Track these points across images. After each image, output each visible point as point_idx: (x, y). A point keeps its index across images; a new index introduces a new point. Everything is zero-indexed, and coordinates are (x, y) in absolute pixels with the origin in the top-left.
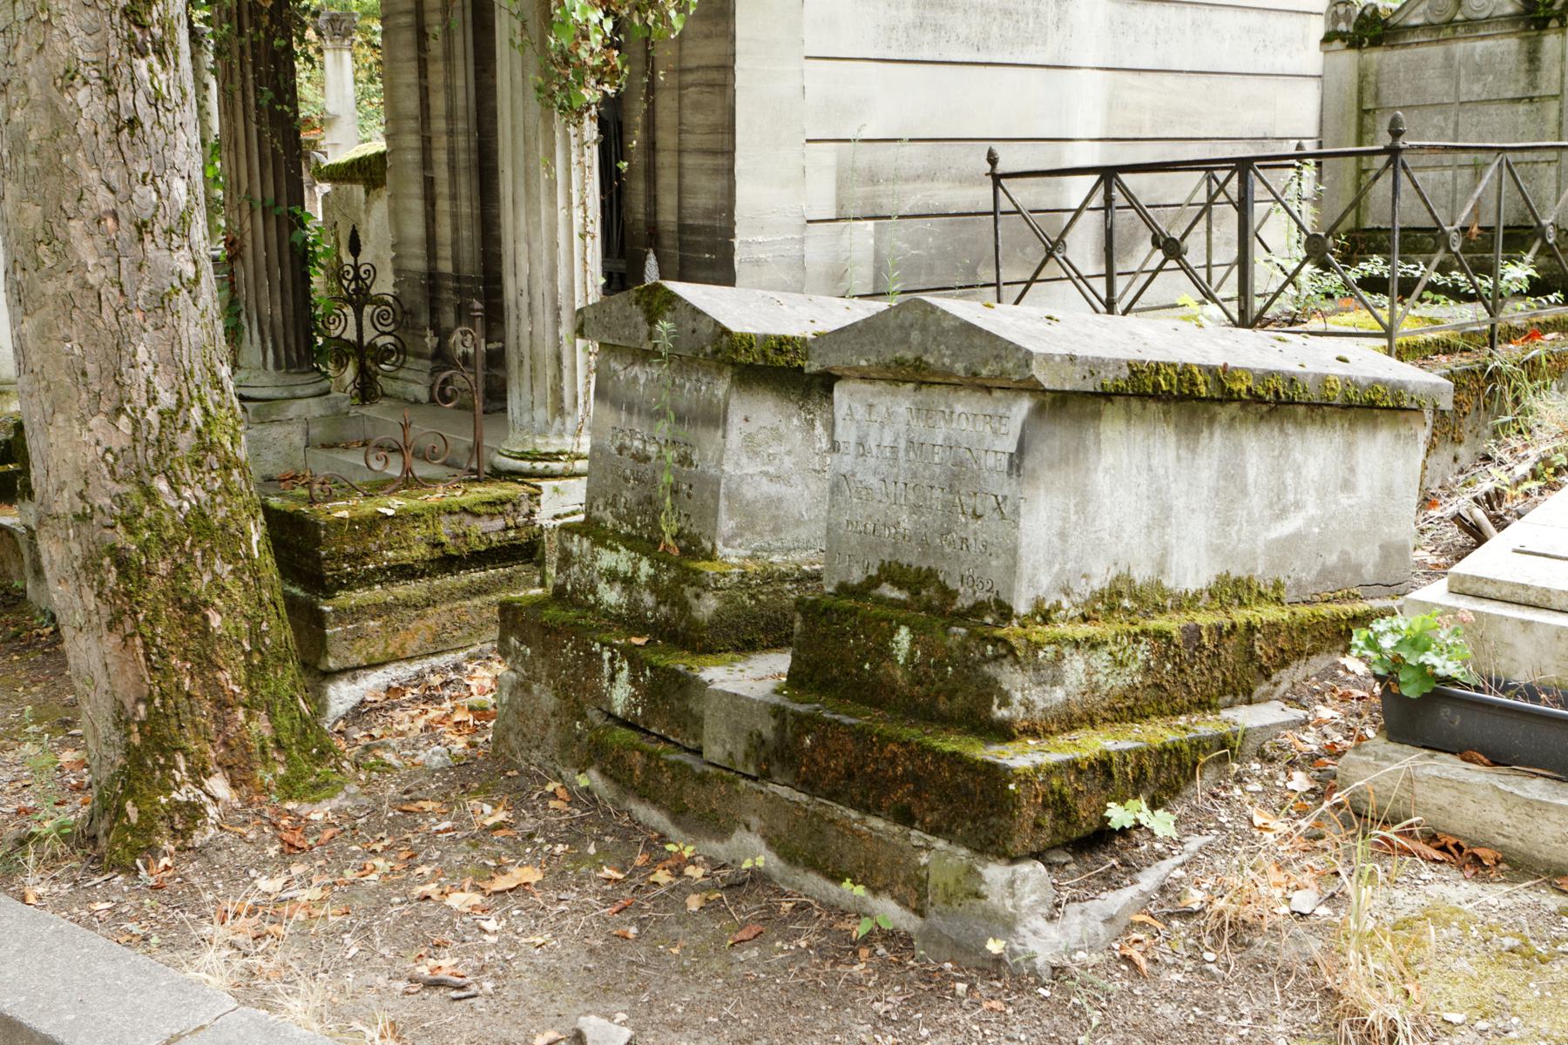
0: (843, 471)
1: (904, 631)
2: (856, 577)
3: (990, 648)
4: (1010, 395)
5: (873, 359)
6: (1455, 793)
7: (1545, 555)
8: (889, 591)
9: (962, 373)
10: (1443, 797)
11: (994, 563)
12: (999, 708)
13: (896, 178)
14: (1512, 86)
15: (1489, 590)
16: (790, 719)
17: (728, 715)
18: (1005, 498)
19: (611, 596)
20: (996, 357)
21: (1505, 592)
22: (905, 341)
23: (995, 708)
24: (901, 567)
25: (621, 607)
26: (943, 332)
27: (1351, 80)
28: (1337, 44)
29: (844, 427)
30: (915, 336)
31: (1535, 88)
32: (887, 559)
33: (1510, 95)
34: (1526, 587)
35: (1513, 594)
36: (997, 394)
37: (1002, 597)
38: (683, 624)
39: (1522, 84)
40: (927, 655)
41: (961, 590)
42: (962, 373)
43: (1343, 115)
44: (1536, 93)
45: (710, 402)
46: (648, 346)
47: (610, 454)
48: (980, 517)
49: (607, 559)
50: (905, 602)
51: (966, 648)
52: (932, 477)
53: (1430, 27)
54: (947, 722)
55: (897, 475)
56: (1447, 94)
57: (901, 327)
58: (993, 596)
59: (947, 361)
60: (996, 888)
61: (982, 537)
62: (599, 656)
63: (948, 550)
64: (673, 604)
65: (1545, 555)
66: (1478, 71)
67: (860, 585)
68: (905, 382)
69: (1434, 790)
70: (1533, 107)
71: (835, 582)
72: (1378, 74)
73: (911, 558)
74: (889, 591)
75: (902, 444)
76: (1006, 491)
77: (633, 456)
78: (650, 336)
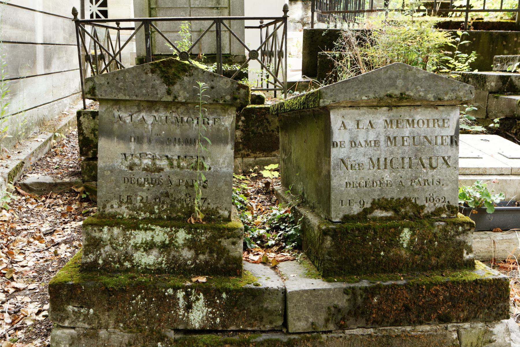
0: (341, 157)
1: (406, 230)
2: (356, 209)
3: (460, 228)
4: (449, 108)
5: (372, 96)
6: (508, 243)
7: (469, 158)
8: (379, 213)
9: (432, 99)
10: (504, 246)
11: (445, 189)
12: (467, 254)
14: (210, 3)
15: (467, 172)
16: (359, 292)
17: (310, 302)
18: (449, 157)
19: (149, 259)
20: (452, 90)
21: (472, 171)
22: (393, 85)
23: (465, 255)
24: (386, 200)
25: (161, 263)
26: (418, 79)
29: (339, 134)
30: (400, 83)
31: (219, 4)
32: (377, 198)
33: (210, 6)
34: (479, 168)
35: (475, 172)
36: (441, 108)
37: (451, 204)
38: (222, 262)
39: (214, 2)
40: (422, 239)
41: (427, 205)
42: (432, 99)
43: (143, 9)
44: (220, 6)
45: (218, 130)
46: (170, 99)
47: (121, 171)
48: (435, 168)
49: (140, 237)
50: (390, 217)
51: (446, 231)
52: (404, 153)
54: (440, 268)
55: (380, 155)
56: (185, 4)
57: (390, 78)
58: (446, 204)
59: (422, 94)
60: (501, 335)
61: (436, 178)
62: (174, 297)
63: (416, 187)
64: (211, 252)
65: (469, 158)
67: (359, 214)
68: (381, 107)
69: (501, 244)
70: (219, 11)
71: (341, 215)
73: (393, 194)
74: (379, 213)
75: (382, 139)
76: (450, 154)
77: (144, 169)
78: (169, 93)
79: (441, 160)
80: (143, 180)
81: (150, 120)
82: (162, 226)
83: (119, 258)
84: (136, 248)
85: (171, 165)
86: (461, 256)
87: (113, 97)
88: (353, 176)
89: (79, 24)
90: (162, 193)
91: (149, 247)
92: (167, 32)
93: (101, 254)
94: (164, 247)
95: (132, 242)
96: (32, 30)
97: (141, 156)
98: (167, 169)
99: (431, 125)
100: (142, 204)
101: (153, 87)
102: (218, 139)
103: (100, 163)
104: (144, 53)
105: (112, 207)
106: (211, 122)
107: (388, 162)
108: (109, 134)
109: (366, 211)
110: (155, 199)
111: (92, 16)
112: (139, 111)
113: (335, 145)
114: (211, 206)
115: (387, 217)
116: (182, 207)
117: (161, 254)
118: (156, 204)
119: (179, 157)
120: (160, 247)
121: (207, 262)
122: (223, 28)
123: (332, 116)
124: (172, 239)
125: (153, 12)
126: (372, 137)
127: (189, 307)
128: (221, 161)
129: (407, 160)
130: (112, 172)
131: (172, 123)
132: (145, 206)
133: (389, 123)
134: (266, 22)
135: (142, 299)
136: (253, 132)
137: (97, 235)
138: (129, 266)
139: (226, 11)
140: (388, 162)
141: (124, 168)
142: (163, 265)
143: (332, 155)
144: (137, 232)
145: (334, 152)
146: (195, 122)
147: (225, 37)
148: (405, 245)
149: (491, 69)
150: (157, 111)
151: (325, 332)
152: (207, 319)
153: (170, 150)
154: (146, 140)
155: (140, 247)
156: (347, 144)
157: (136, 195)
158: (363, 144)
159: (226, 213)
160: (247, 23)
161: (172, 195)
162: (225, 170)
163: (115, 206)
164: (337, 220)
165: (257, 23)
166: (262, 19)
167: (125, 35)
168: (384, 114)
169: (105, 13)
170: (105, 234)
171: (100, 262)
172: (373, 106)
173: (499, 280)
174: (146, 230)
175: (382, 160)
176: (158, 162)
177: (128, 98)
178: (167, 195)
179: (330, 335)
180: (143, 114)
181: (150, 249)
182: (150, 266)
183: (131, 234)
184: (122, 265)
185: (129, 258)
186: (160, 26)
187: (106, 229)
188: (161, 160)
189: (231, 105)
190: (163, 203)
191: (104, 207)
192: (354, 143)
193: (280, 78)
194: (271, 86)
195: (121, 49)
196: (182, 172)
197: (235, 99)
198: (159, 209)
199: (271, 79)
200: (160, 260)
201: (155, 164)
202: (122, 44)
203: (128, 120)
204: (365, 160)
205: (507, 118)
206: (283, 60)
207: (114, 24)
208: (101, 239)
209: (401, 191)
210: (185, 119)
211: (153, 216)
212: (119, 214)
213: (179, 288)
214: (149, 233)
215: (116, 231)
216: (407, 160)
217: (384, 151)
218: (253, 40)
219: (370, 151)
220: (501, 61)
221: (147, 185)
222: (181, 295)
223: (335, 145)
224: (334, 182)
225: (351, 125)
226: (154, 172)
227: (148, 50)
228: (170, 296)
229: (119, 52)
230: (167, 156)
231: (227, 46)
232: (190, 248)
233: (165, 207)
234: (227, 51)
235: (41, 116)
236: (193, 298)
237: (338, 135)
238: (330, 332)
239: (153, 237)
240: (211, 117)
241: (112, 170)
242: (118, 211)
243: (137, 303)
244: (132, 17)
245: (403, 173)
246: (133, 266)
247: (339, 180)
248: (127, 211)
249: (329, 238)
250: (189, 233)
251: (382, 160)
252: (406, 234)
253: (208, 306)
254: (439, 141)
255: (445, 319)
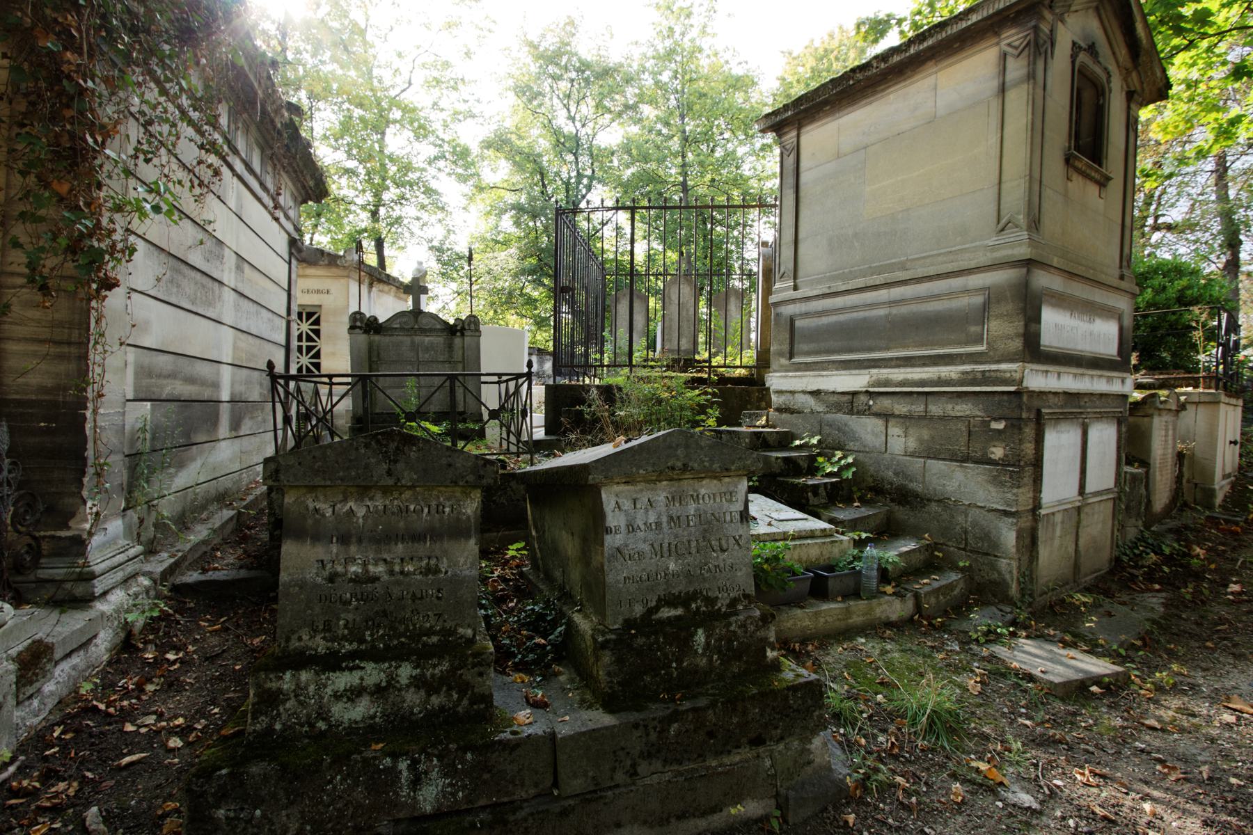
0: (616, 546)
1: (700, 631)
13: (159, 376)
27: (364, 348)
28: (357, 331)
45: (458, 519)
46: (390, 482)
47: (316, 586)
49: (342, 680)
52: (690, 535)
53: (402, 329)
61: (729, 562)
62: (393, 772)
63: (707, 575)
66: (427, 350)
72: (378, 347)
73: (680, 588)
74: (666, 613)
75: (664, 519)
76: (741, 532)
77: (351, 580)
79: (732, 541)
80: (348, 595)
81: (361, 512)
82: (376, 662)
83: (308, 716)
84: (337, 696)
85: (391, 573)
86: (765, 656)
87: (306, 483)
88: (632, 568)
89: (274, 377)
90: (377, 612)
91: (353, 694)
92: (390, 387)
93: (279, 715)
94: (379, 692)
95: (329, 690)
96: (216, 385)
97: (350, 560)
98: (386, 577)
99: (718, 500)
100: (346, 632)
101: (367, 467)
102: (457, 531)
103: (284, 577)
104: (360, 411)
105: (300, 639)
106: (447, 510)
107: (673, 547)
108: (300, 535)
109: (651, 611)
110: (367, 622)
111: (300, 369)
112: (345, 500)
113: (608, 531)
114: (448, 625)
115: (676, 617)
116: (407, 629)
117: (372, 702)
118: (368, 629)
119: (402, 560)
120: (372, 694)
121: (442, 708)
122: (457, 384)
123: (604, 496)
124: (392, 679)
125: (374, 366)
126: (652, 518)
127: (416, 783)
128: (462, 560)
129: (694, 544)
130: (301, 588)
131: (393, 513)
132: (351, 633)
133: (674, 498)
134: (504, 378)
135: (344, 779)
136: (494, 502)
137: (274, 685)
138: (323, 728)
139: (460, 366)
140: (673, 547)
141: (319, 580)
142: (377, 720)
143: (606, 544)
144: (338, 674)
145: (608, 539)
146: (426, 510)
147: (459, 392)
148: (700, 651)
149: (740, 425)
150: (371, 499)
151: (610, 788)
152: (444, 796)
153: (390, 551)
154: (354, 540)
155: (341, 696)
156: (623, 528)
157: (339, 619)
158: (642, 527)
159: (469, 632)
160: (483, 379)
161: (391, 613)
162: (467, 572)
163: (305, 637)
164: (616, 627)
165: (495, 379)
166: (500, 375)
167: (339, 390)
168: (664, 490)
169: (317, 366)
170: (287, 681)
171: (278, 727)
172: (889, 624)
173: (811, 683)
174: (351, 669)
175: (666, 545)
176: (371, 568)
177: (328, 483)
178: (385, 614)
179: (617, 791)
180: (351, 504)
181: (357, 696)
182: (356, 722)
183: (328, 678)
184: (312, 726)
185: (323, 714)
186: (382, 382)
187: (288, 675)
188: (376, 565)
189: (475, 487)
190: (379, 626)
191: (288, 640)
192: (631, 528)
193: (525, 437)
194: (513, 449)
195: (333, 406)
196: (408, 579)
197: (481, 477)
198: (372, 635)
199: (513, 439)
200: (372, 711)
201: (367, 571)
202: (335, 399)
203: (329, 513)
204: (646, 548)
205: (764, 476)
206: (528, 419)
207: (326, 380)
208: (280, 691)
209: (690, 582)
210: (412, 507)
211: (363, 647)
212: (311, 649)
213: (401, 755)
214: (357, 674)
215: (304, 676)
216: (694, 544)
217: (667, 535)
218: (491, 397)
219: (651, 536)
220: (750, 416)
221: (354, 603)
222: (403, 765)
223: (608, 531)
224: (610, 578)
225: (627, 505)
226: (366, 583)
227: (365, 410)
228: (386, 769)
229: (331, 410)
230: (385, 560)
231: (462, 403)
232: (418, 688)
233: (381, 632)
234: (461, 409)
235: (221, 489)
236: (422, 767)
237: (614, 519)
238: (617, 786)
239: (362, 679)
240: (448, 504)
241: (302, 585)
242: (310, 644)
243: (335, 788)
244: (349, 372)
245: (690, 559)
246: (331, 726)
247: (616, 575)
248: (322, 642)
249: (608, 653)
250: (415, 668)
251: (666, 545)
252: (700, 636)
253: (446, 776)
254: (728, 518)
255: (757, 742)
